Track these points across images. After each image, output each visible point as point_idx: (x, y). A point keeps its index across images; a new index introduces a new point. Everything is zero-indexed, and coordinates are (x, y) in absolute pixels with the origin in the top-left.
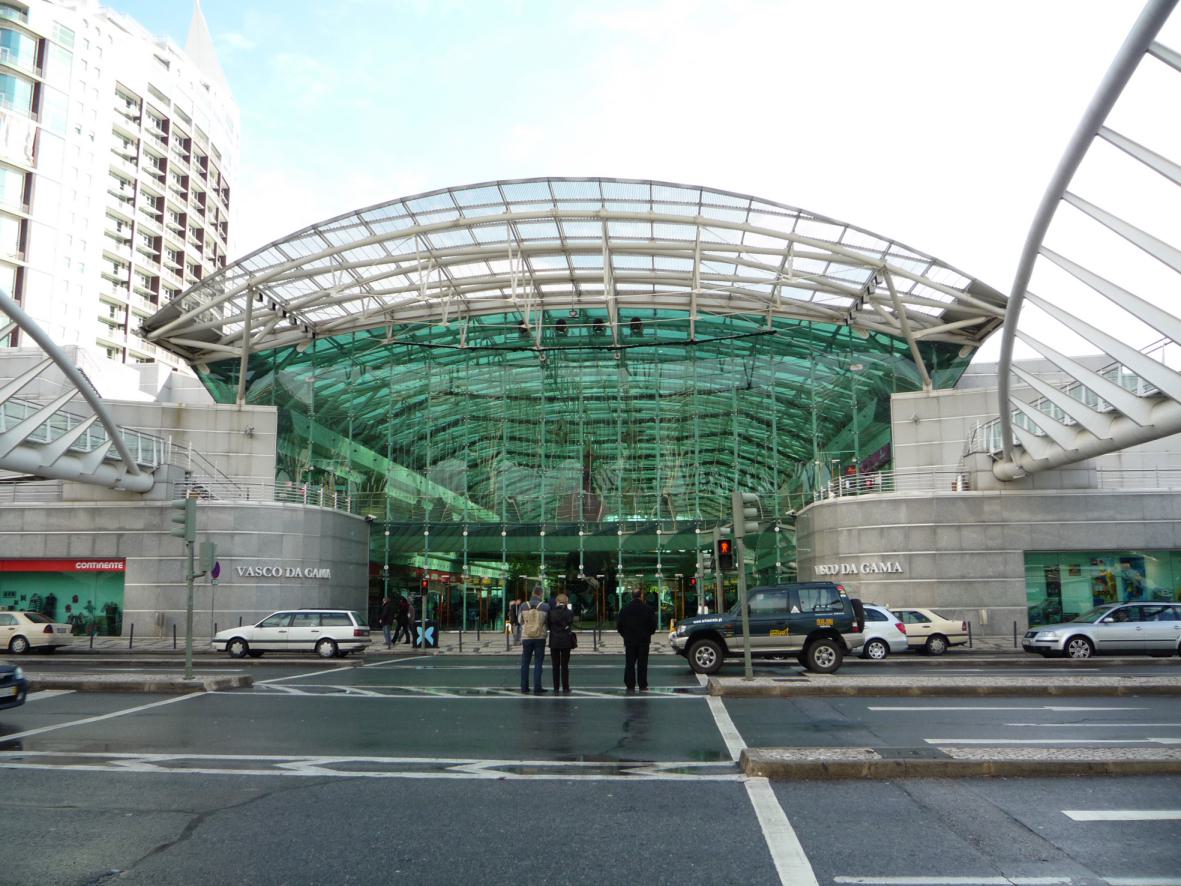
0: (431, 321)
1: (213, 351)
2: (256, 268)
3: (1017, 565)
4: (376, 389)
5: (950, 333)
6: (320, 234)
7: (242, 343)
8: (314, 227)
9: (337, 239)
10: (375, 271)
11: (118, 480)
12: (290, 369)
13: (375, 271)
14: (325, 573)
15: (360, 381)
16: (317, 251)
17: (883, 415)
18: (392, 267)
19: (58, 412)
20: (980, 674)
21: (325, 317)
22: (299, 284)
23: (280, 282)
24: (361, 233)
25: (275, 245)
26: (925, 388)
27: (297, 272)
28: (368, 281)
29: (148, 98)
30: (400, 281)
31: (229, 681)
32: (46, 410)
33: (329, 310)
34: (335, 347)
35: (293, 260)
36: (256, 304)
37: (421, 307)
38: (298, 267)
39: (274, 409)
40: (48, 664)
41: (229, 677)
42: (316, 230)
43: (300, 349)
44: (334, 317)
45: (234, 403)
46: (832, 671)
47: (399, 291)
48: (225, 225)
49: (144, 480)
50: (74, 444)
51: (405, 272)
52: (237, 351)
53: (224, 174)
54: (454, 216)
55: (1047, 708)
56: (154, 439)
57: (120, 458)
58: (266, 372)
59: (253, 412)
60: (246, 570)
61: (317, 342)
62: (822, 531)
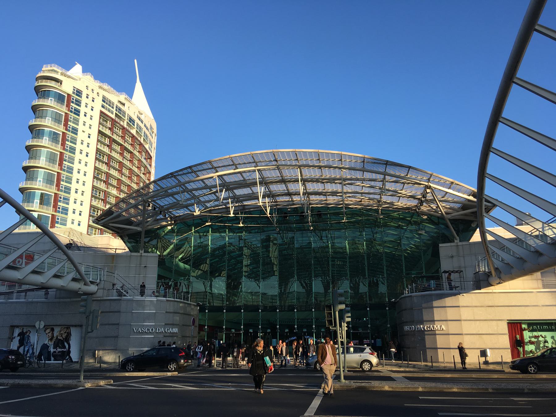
3: (504, 328)
5: (465, 215)
6: (175, 177)
8: (171, 174)
10: (200, 192)
11: (79, 288)
16: (174, 184)
17: (436, 254)
19: (49, 257)
26: (456, 241)
27: (166, 193)
29: (137, 121)
35: (163, 188)
38: (166, 191)
45: (139, 252)
55: (512, 398)
56: (91, 267)
57: (81, 278)
59: (147, 256)
60: (138, 329)
62: (405, 310)
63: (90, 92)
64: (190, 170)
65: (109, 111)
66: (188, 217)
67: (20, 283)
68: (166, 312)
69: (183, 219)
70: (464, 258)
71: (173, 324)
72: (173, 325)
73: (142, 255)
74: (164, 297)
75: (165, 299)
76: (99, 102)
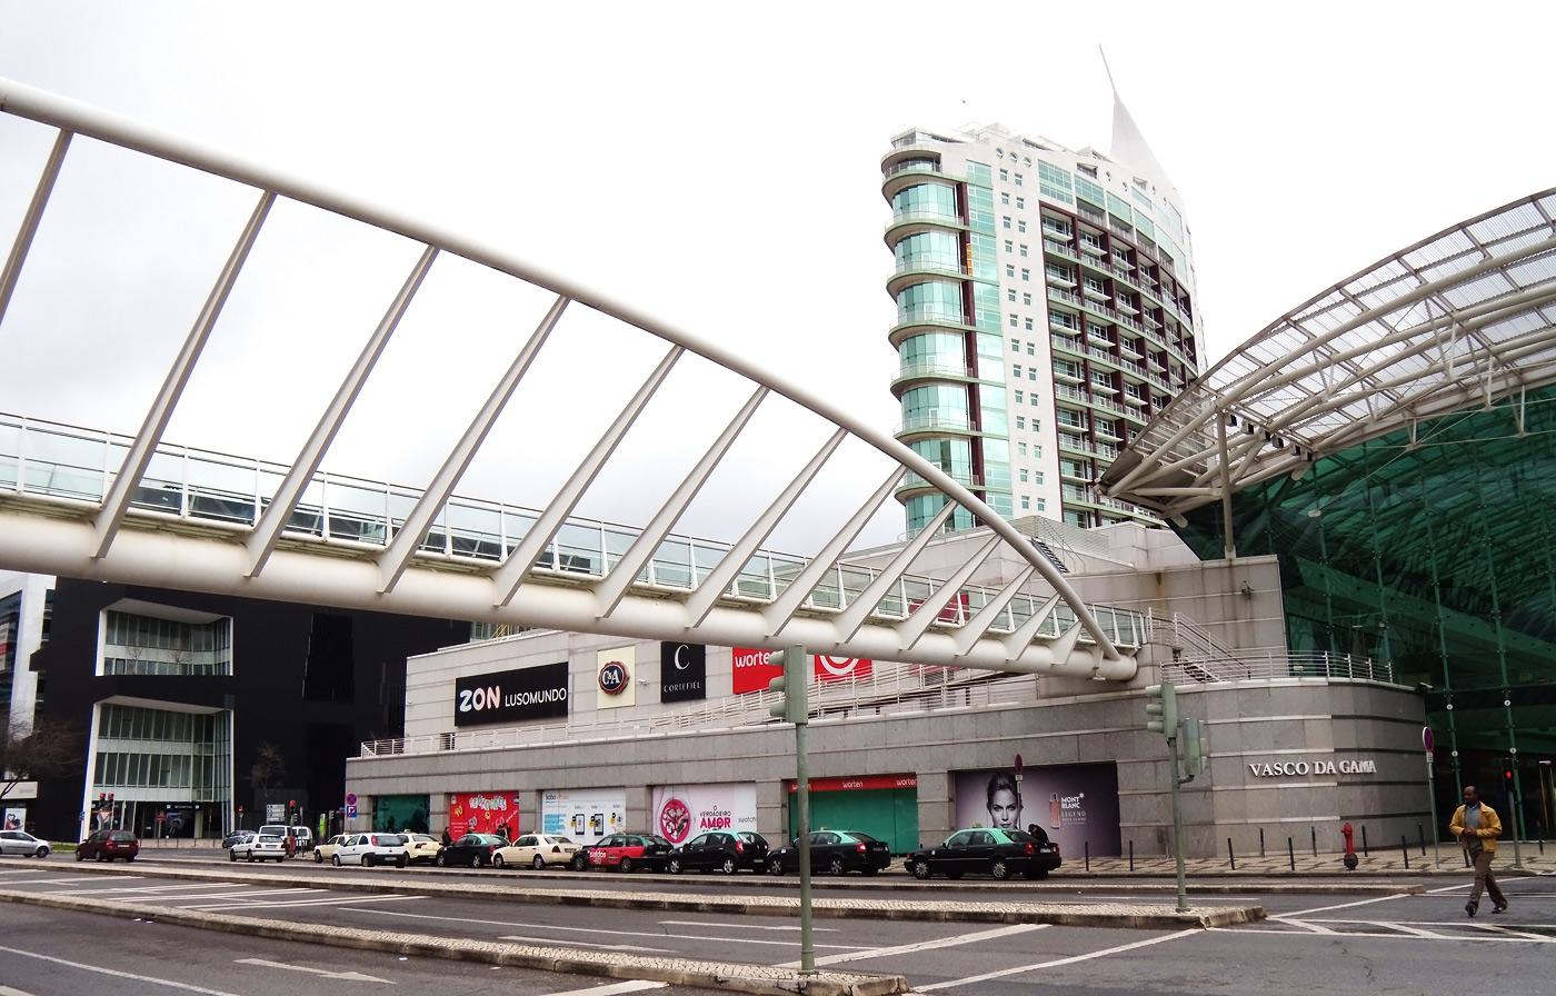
0: (1469, 409)
1: (1188, 497)
2: (1223, 385)
4: (1410, 514)
7: (1218, 482)
8: (1286, 318)
9: (1318, 327)
10: (1377, 357)
11: (1096, 668)
12: (1288, 504)
13: (1377, 357)
14: (1367, 766)
15: (1384, 505)
18: (1401, 346)
20: (1130, 902)
21: (1322, 431)
22: (1280, 394)
23: (1254, 397)
24: (1349, 313)
25: (1240, 351)
27: (1273, 378)
28: (1371, 373)
30: (1415, 364)
31: (1233, 914)
32: (947, 587)
33: (1325, 420)
34: (1342, 467)
35: (1267, 365)
36: (1230, 430)
37: (1451, 392)
39: (1273, 558)
40: (1035, 891)
41: (1233, 909)
42: (1288, 321)
43: (1296, 477)
44: (1333, 427)
45: (1224, 558)
46: (732, 874)
47: (1416, 378)
48: (1191, 341)
49: (1125, 665)
50: (992, 624)
51: (1378, 316)
52: (1215, 492)
53: (1179, 278)
54: (1476, 259)
58: (1258, 513)
59: (1248, 565)
61: (1317, 465)
63: (1007, 163)
64: (1337, 296)
65: (1061, 197)
66: (1345, 439)
67: (956, 664)
68: (1334, 717)
69: (1331, 445)
70: (1231, 573)
71: (1360, 750)
72: (1361, 751)
73: (1234, 563)
74: (1318, 675)
75: (1323, 679)
76: (1032, 178)
